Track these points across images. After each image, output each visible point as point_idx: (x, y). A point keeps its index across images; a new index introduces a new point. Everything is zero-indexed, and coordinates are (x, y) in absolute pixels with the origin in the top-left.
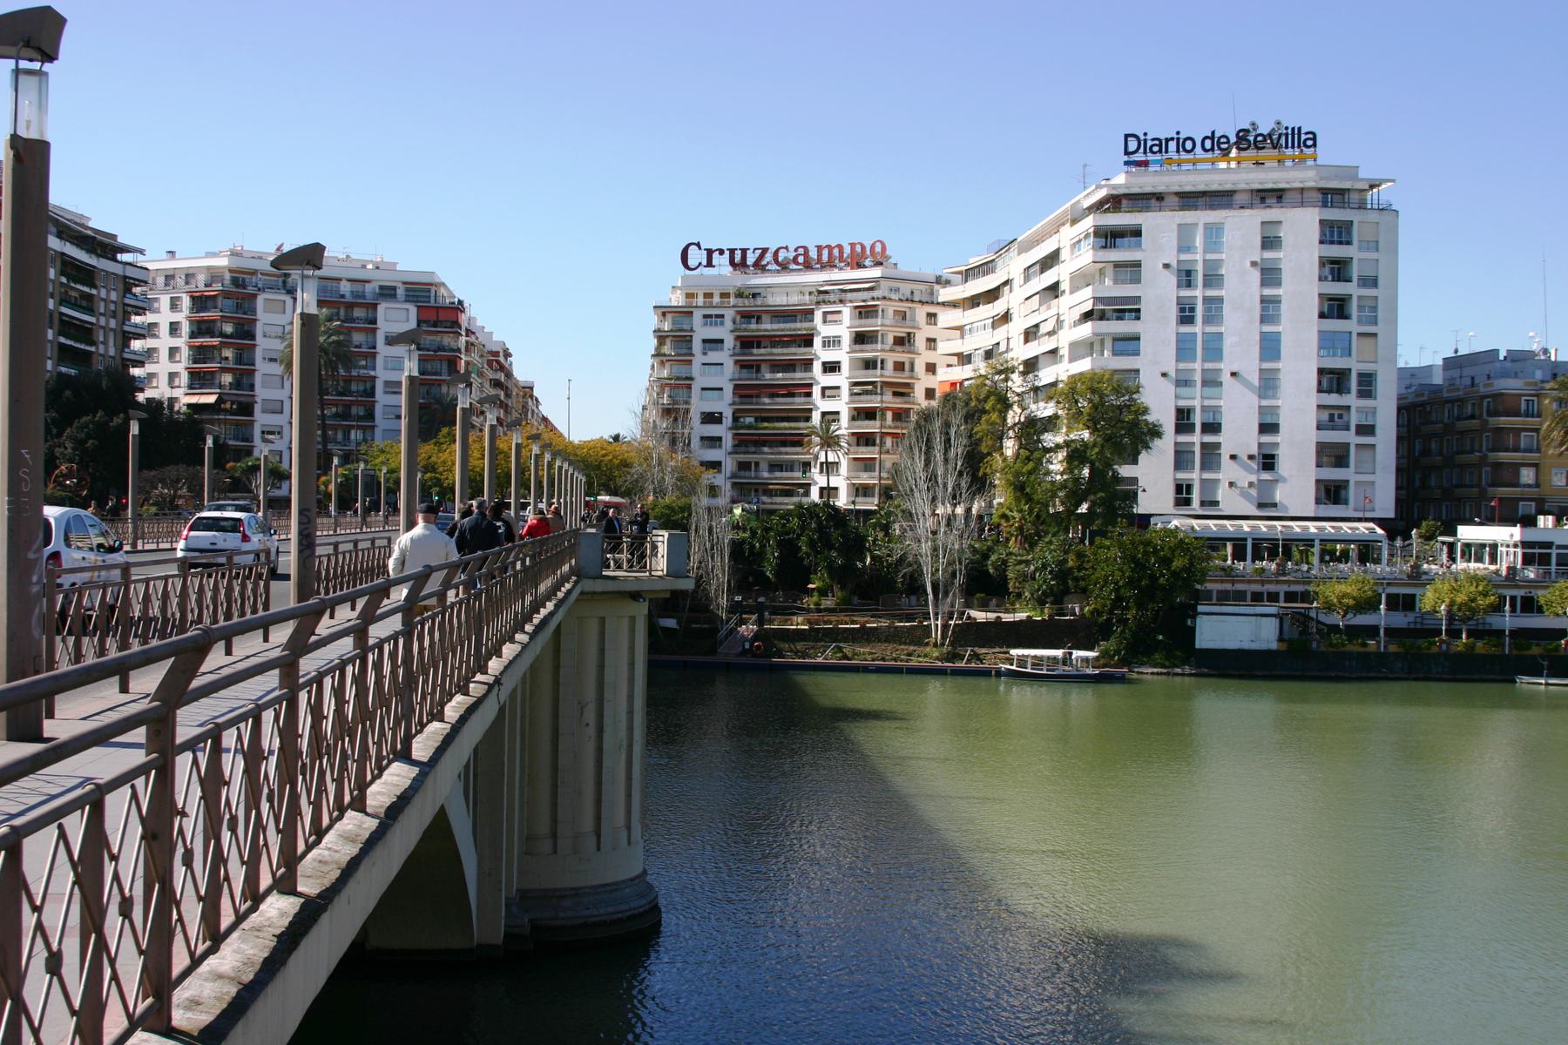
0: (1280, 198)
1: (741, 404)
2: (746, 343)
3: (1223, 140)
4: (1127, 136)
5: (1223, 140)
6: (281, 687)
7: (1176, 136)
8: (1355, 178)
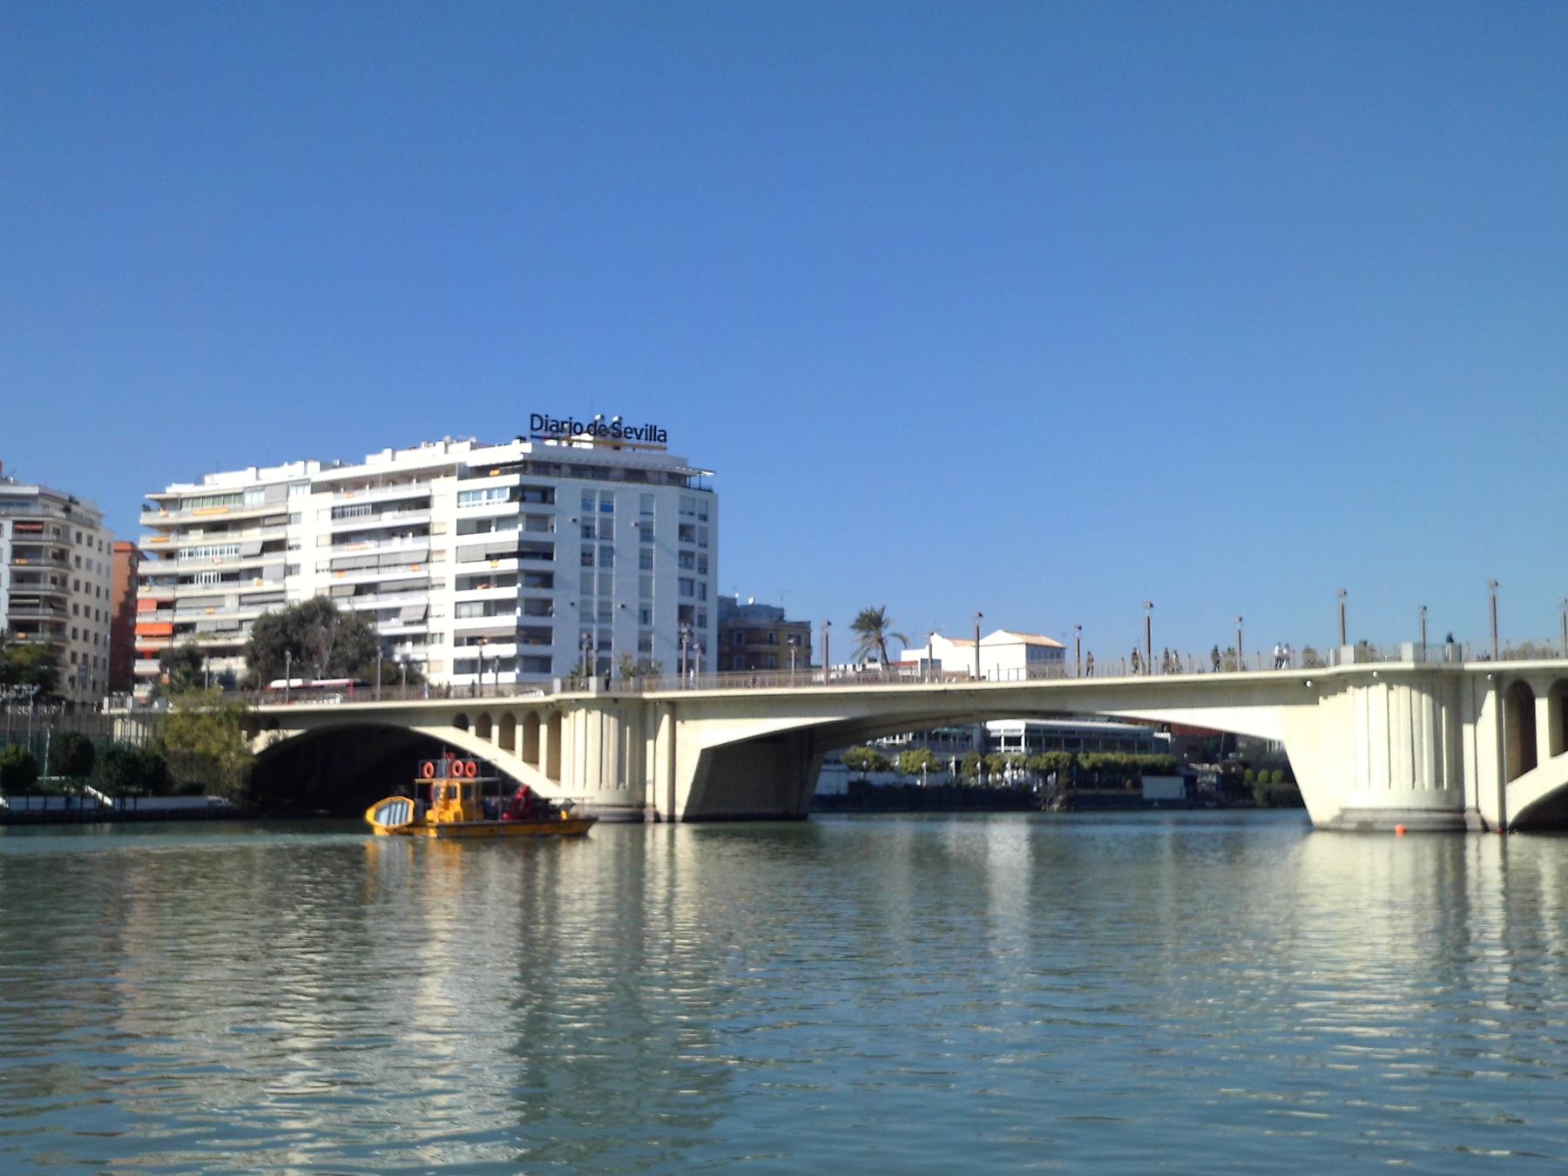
4: (533, 416)
6: (820, 770)
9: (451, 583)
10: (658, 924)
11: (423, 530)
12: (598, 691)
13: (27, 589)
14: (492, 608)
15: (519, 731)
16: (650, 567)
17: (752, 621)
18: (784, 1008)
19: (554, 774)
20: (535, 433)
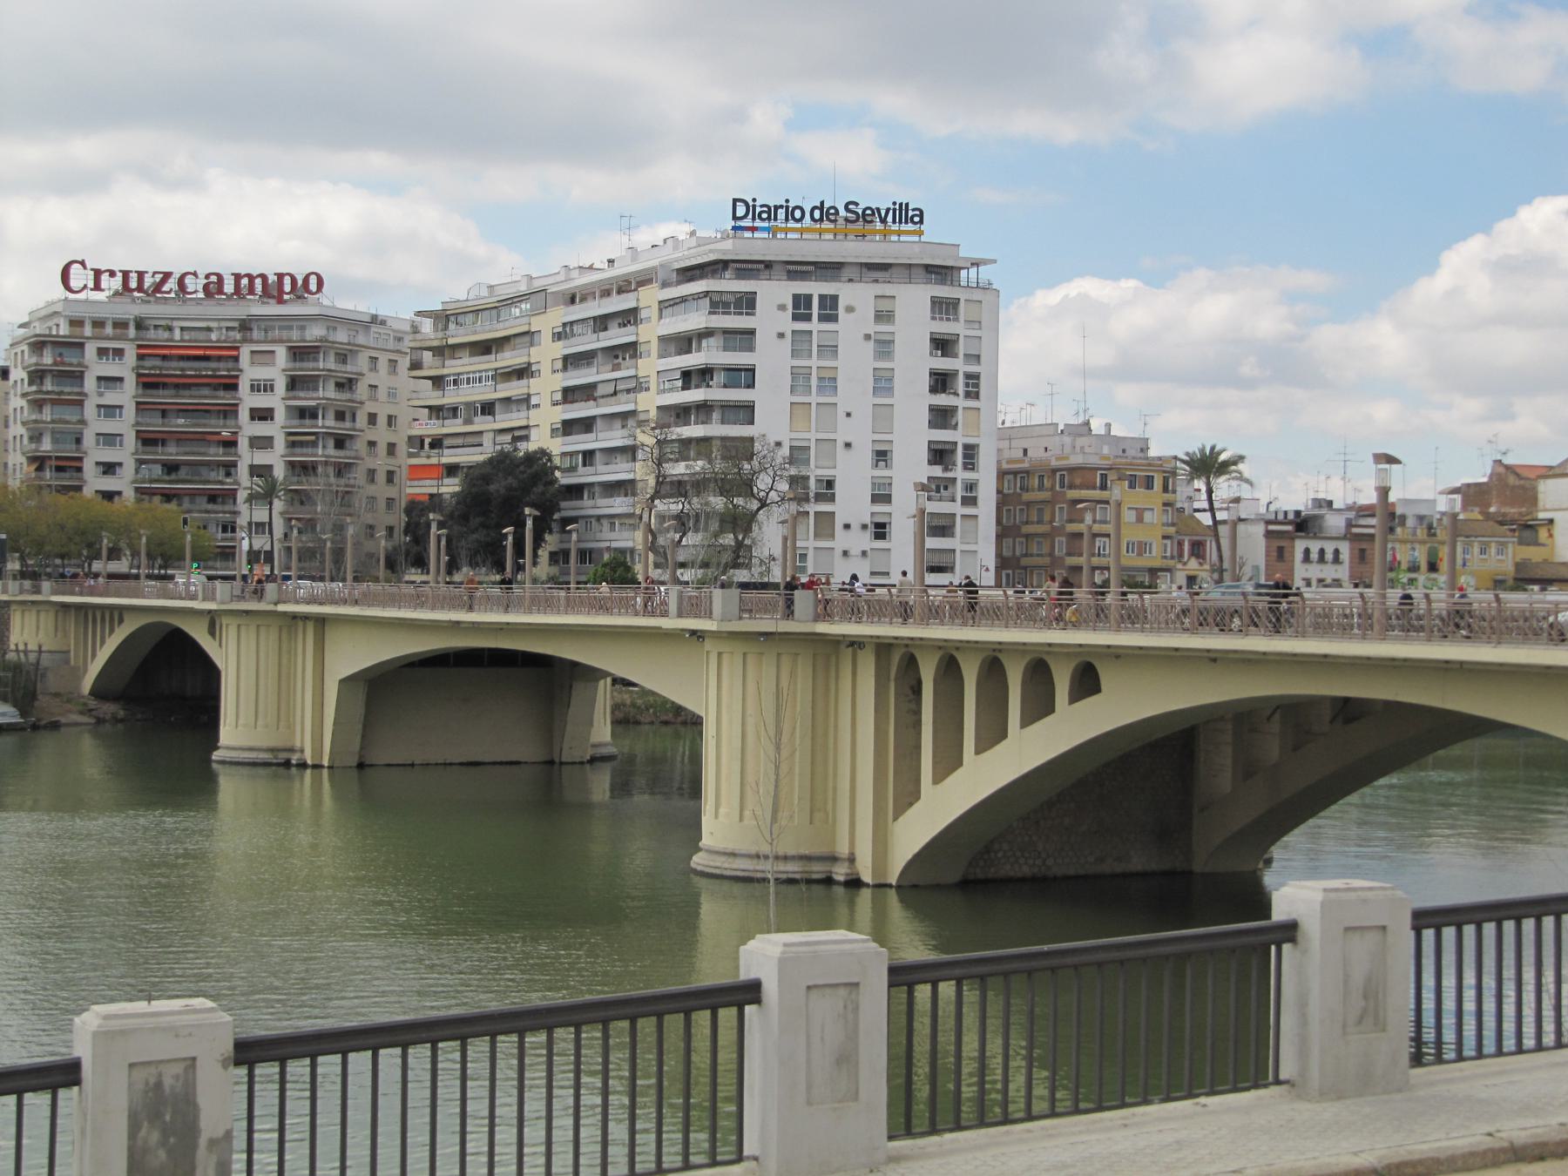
1: (144, 453)
3: (832, 211)
4: (735, 201)
5: (832, 211)
7: (785, 204)
13: (307, 426)
16: (889, 391)
20: (740, 223)
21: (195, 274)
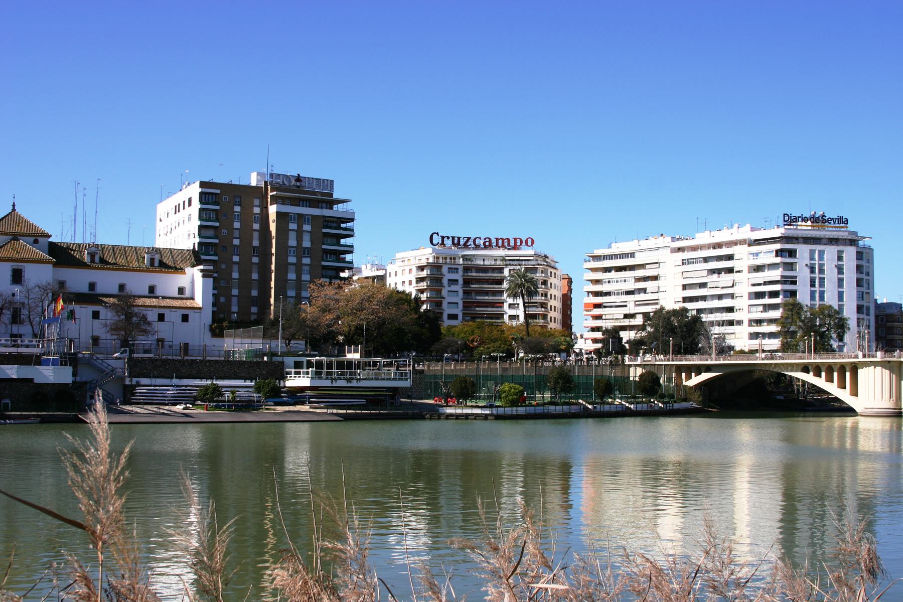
0: (836, 242)
2: (467, 282)
4: (784, 215)
8: (857, 235)
9: (746, 270)
10: (300, 347)
11: (730, 270)
12: (881, 358)
14: (767, 308)
15: (835, 375)
17: (888, 311)
18: (188, 573)
19: (854, 392)
21: (480, 238)
